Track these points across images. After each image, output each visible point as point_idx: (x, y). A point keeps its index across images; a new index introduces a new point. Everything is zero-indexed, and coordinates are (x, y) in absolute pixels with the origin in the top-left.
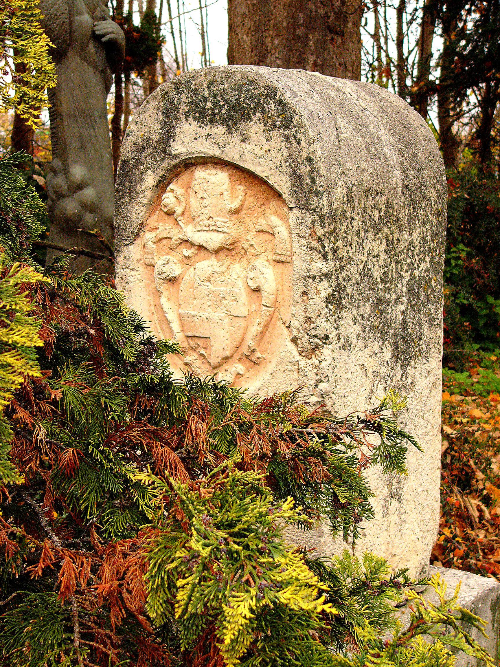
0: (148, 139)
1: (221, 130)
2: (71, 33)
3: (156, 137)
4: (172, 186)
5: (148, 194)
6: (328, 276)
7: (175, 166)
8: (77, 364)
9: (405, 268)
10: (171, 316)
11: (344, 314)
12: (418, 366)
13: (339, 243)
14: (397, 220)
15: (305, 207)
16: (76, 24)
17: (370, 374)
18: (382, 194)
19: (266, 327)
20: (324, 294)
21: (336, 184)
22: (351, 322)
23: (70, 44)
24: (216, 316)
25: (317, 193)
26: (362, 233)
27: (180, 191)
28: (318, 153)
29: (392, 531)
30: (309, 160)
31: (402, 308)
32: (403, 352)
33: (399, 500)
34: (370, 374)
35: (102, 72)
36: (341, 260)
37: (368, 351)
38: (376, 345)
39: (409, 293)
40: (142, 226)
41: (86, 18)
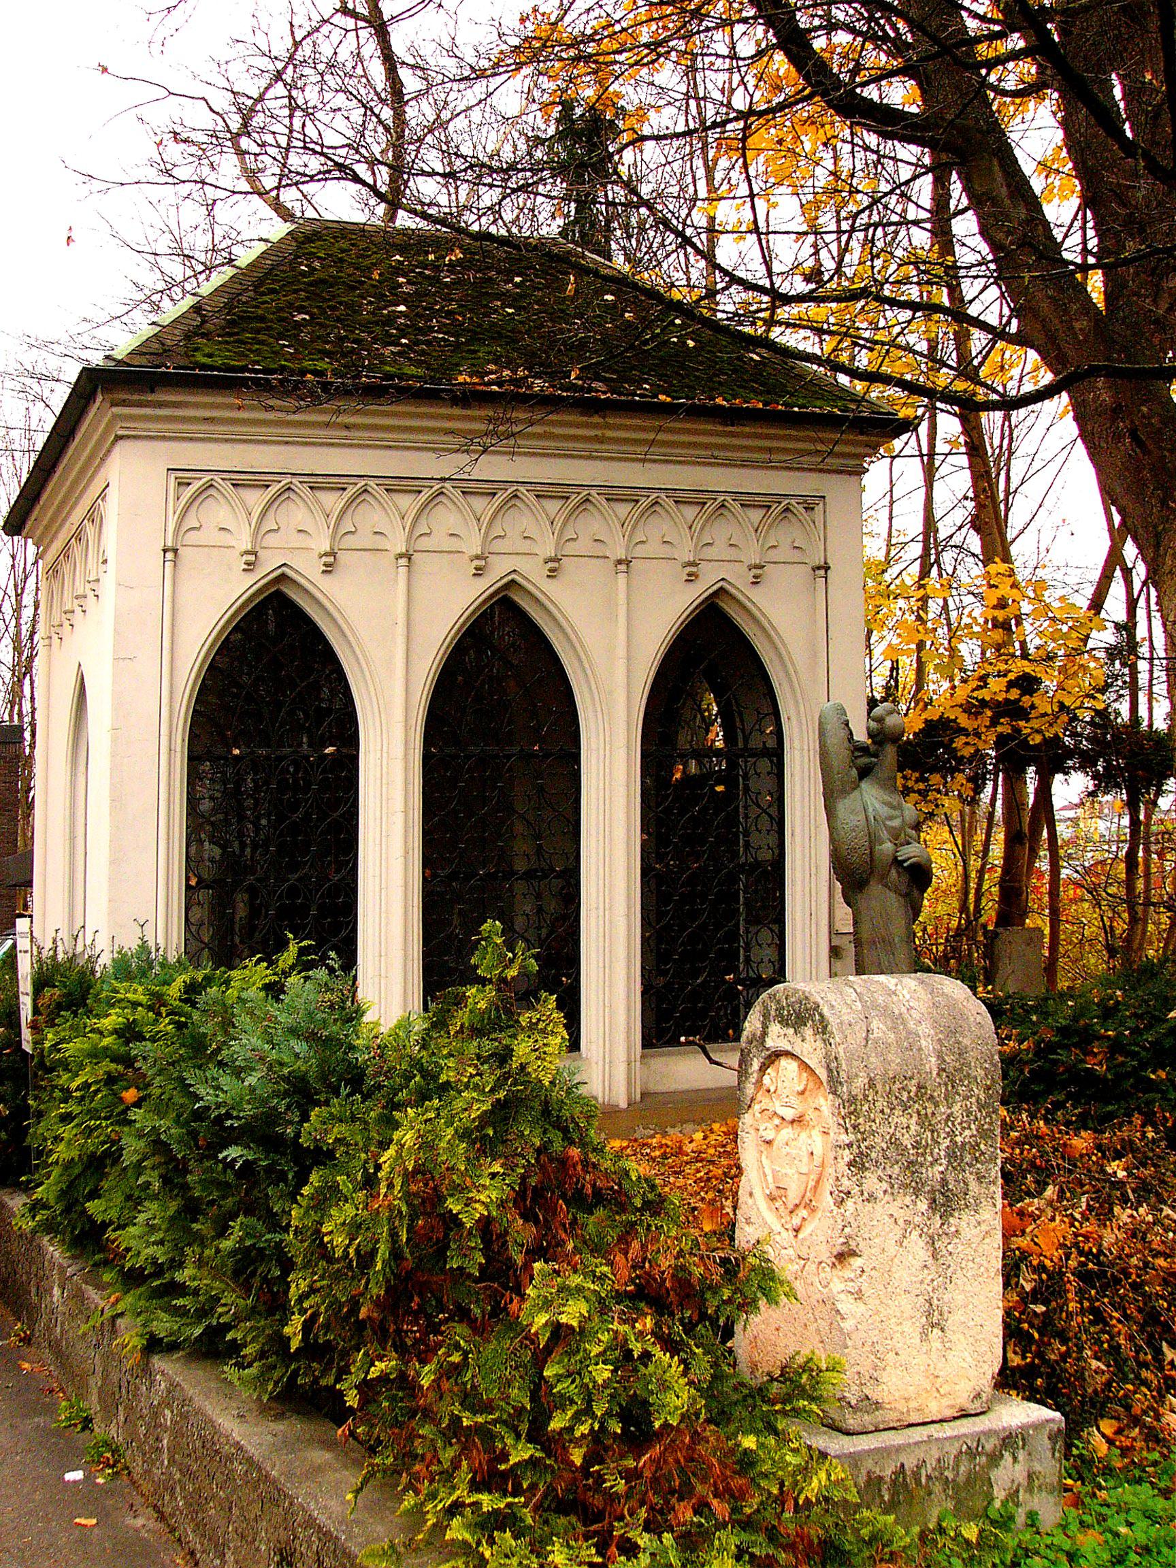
0: (754, 1035)
1: (792, 1031)
2: (872, 860)
3: (758, 1033)
4: (769, 1070)
5: (755, 1075)
6: (850, 1146)
7: (770, 1056)
8: (604, 1207)
9: (943, 1135)
10: (768, 1171)
11: (867, 1174)
12: (964, 1217)
13: (861, 1120)
14: (932, 1097)
15: (834, 1093)
16: (877, 856)
17: (901, 1222)
18: (911, 1078)
19: (818, 1182)
20: (847, 1159)
21: (857, 1075)
22: (876, 1180)
23: (872, 872)
24: (791, 1172)
25: (841, 1083)
26: (887, 1111)
27: (773, 1074)
28: (842, 1054)
29: (934, 1355)
30: (836, 1058)
31: (941, 1169)
32: (943, 1205)
33: (942, 1330)
34: (901, 1222)
35: (906, 896)
36: (862, 1133)
37: (898, 1203)
38: (908, 1200)
39: (948, 1155)
40: (752, 1100)
41: (888, 846)
